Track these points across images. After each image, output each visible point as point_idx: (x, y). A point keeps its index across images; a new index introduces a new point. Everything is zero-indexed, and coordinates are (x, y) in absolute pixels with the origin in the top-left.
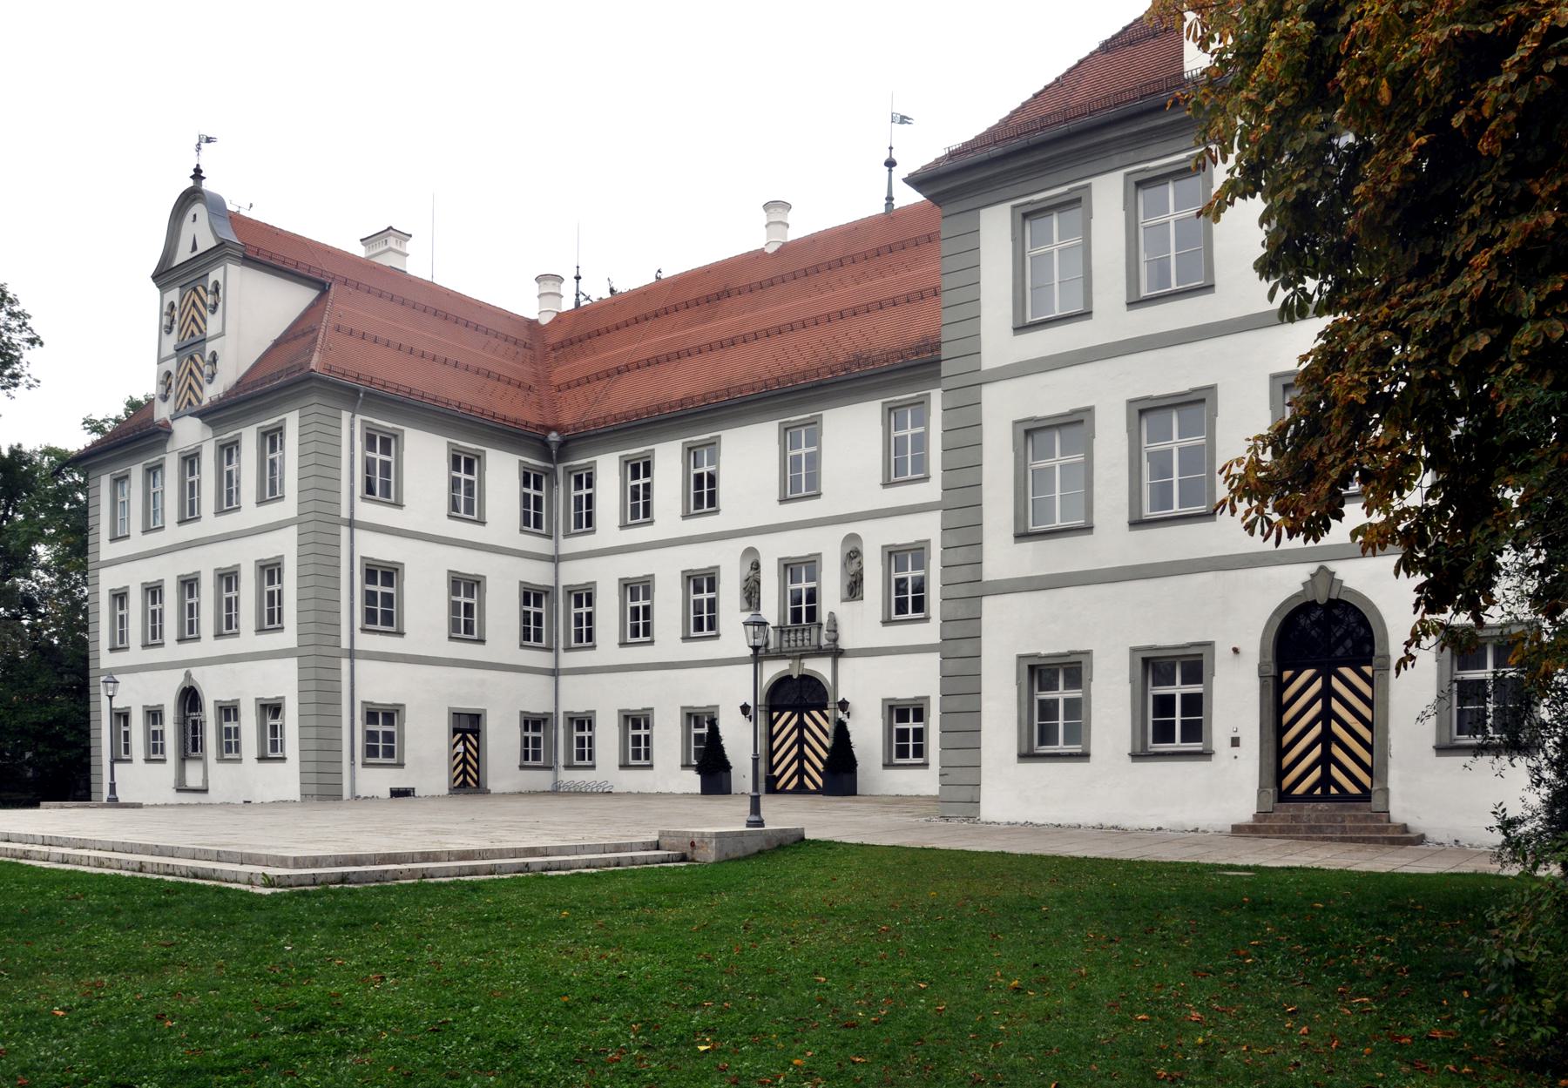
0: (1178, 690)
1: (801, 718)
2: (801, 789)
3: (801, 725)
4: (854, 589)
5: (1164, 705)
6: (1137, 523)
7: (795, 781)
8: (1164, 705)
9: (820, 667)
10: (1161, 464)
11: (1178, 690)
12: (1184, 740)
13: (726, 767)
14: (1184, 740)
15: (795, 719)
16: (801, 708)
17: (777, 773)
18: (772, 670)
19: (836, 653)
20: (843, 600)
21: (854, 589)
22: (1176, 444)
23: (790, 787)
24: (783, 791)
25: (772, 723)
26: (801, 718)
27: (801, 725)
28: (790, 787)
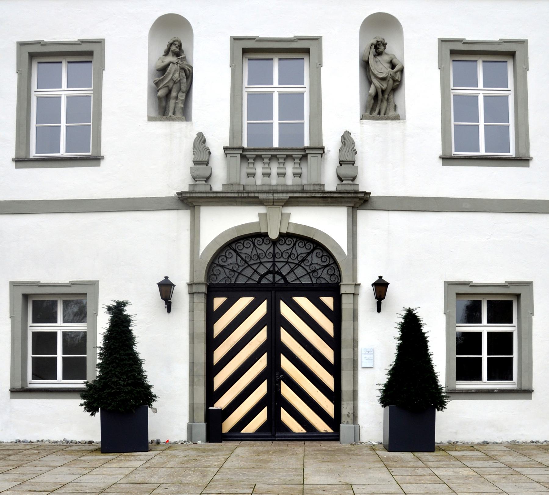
0: (60, 327)
1: (274, 310)
2: (274, 431)
3: (274, 321)
4: (382, 95)
5: (44, 342)
6: (22, 161)
7: (262, 417)
8: (44, 342)
9: (327, 223)
10: (49, 107)
11: (484, 328)
12: (491, 377)
13: (144, 396)
14: (491, 377)
15: (262, 310)
16: (275, 291)
17: (222, 403)
18: (220, 223)
19: (356, 200)
20: (150, 119)
21: (382, 95)
22: (64, 92)
23: (252, 427)
24: (236, 434)
25: (212, 317)
26: (274, 310)
27: (274, 321)
28: (252, 427)
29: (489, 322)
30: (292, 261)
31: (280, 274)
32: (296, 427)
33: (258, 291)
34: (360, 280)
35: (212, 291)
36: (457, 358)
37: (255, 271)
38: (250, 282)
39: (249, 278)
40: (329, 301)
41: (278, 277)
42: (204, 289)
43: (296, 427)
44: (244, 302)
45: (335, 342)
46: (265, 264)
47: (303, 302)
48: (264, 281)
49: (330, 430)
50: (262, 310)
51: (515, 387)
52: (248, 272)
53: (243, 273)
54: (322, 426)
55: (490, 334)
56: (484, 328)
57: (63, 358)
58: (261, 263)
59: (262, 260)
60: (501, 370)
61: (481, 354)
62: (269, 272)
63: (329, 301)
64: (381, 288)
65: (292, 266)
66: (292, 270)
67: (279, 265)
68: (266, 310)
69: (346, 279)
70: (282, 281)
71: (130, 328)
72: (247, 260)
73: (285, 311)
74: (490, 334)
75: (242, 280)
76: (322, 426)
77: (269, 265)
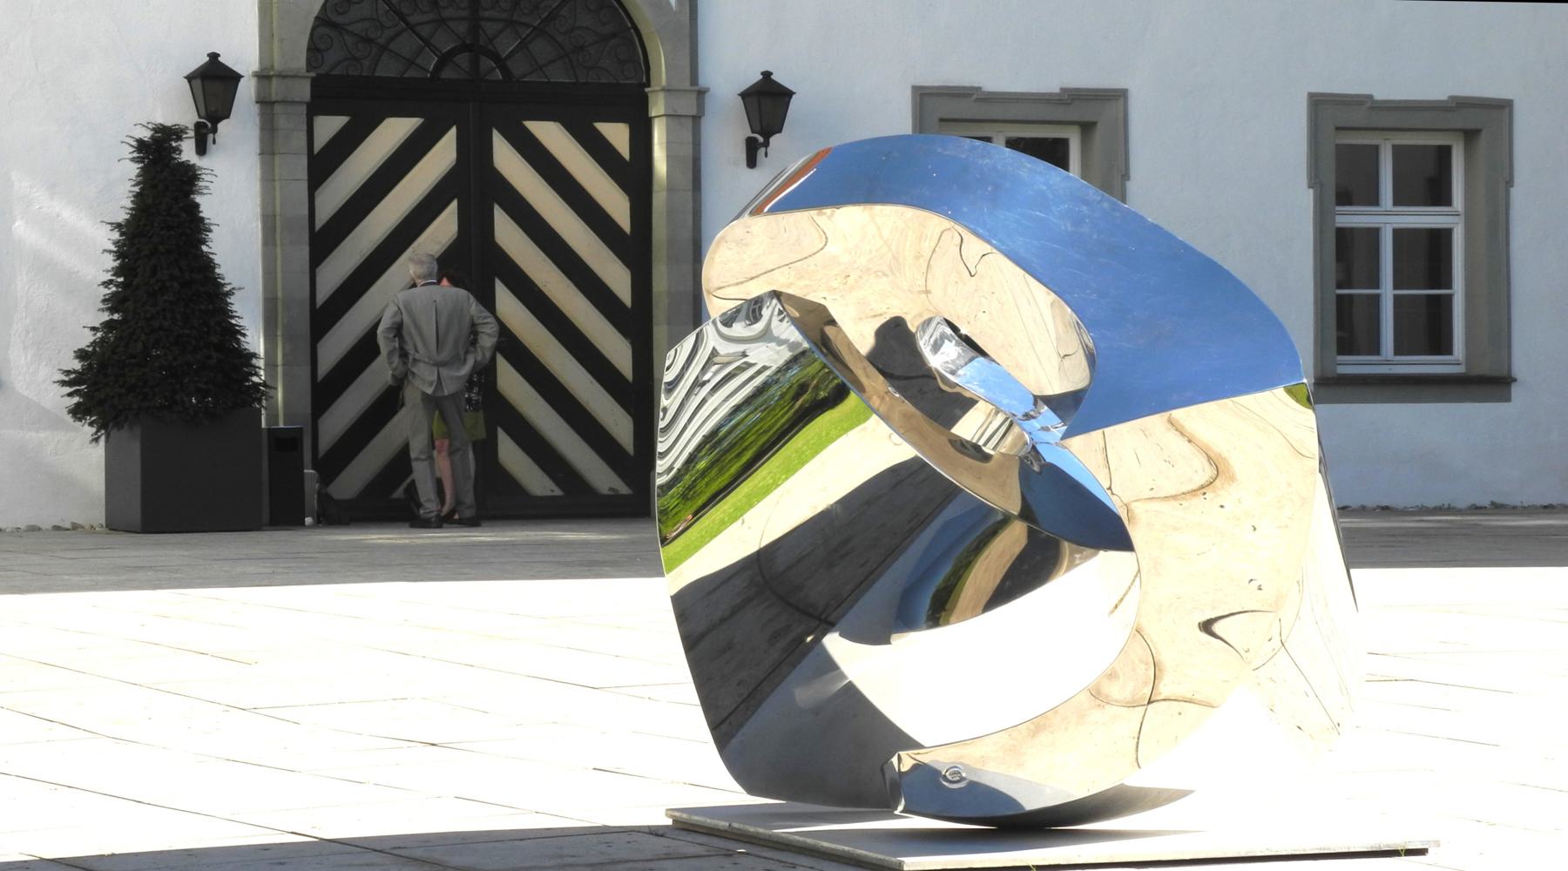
1: (474, 156)
3: (475, 187)
11: (1389, 218)
15: (442, 156)
26: (474, 156)
27: (475, 187)
29: (1396, 202)
30: (523, 20)
31: (495, 57)
32: (536, 482)
33: (435, 104)
34: (708, 76)
35: (323, 98)
36: (1339, 297)
37: (428, 44)
38: (412, 73)
39: (411, 63)
40: (617, 134)
41: (486, 63)
42: (304, 91)
43: (536, 482)
44: (393, 132)
45: (634, 247)
46: (451, 24)
47: (551, 135)
48: (448, 74)
49: (624, 489)
50: (442, 156)
51: (1460, 370)
52: (406, 44)
53: (392, 46)
54: (602, 478)
55: (1398, 234)
56: (1389, 218)
57: (1378, 287)
58: (442, 22)
59: (446, 13)
60: (1428, 327)
61: (1378, 287)
62: (463, 48)
63: (617, 134)
64: (768, 103)
65: (525, 32)
66: (524, 45)
67: (490, 28)
68: (454, 155)
69: (661, 70)
70: (498, 75)
71: (198, 199)
72: (405, 11)
73: (507, 160)
74: (1398, 234)
75: (388, 69)
76: (602, 478)
77: (462, 28)
